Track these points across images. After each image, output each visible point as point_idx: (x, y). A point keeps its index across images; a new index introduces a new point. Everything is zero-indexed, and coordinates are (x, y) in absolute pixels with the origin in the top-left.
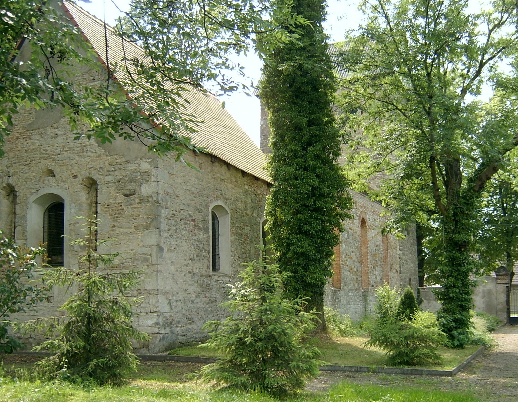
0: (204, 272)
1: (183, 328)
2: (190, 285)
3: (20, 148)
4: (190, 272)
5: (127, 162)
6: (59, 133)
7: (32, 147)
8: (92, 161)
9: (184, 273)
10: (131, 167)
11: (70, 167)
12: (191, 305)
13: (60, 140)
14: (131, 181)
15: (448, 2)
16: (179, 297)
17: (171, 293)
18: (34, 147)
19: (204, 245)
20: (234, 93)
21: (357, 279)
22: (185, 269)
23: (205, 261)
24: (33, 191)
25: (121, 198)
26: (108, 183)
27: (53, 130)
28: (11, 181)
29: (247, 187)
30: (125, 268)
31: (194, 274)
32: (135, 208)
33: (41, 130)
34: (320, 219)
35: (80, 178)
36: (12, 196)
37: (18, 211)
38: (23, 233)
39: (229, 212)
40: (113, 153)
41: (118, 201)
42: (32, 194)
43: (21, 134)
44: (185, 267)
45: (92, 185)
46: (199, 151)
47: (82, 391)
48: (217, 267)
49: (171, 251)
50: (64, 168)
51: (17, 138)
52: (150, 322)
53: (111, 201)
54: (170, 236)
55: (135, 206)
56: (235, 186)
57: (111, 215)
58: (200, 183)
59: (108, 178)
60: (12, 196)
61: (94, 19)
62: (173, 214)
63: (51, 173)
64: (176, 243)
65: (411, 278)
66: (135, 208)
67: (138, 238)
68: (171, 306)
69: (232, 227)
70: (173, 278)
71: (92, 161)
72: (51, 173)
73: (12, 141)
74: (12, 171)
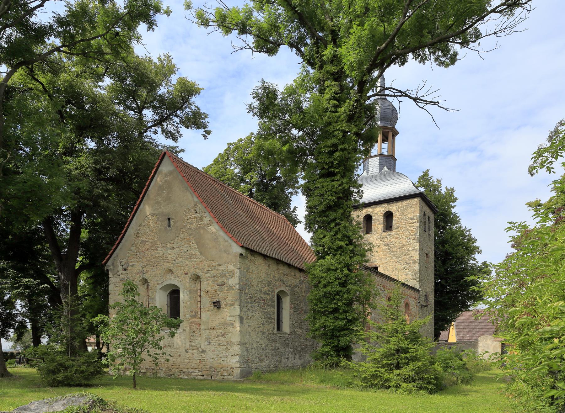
0: (271, 332)
2: (261, 339)
3: (150, 256)
4: (261, 332)
5: (220, 265)
6: (175, 246)
7: (158, 255)
8: (197, 264)
10: (222, 268)
11: (183, 268)
14: (222, 277)
15: (564, 216)
22: (257, 330)
23: (272, 324)
24: (160, 282)
25: (216, 287)
26: (207, 278)
27: (171, 245)
28: (145, 276)
29: (302, 278)
30: (219, 329)
35: (189, 275)
36: (146, 285)
37: (150, 294)
42: (158, 284)
43: (150, 247)
45: (197, 278)
48: (281, 328)
49: (248, 319)
50: (179, 268)
51: (148, 250)
52: (234, 361)
53: (210, 289)
57: (209, 297)
59: (207, 275)
60: (146, 285)
61: (427, 222)
63: (170, 271)
68: (248, 352)
70: (250, 335)
71: (197, 264)
72: (170, 271)
73: (399, 254)
74: (145, 270)
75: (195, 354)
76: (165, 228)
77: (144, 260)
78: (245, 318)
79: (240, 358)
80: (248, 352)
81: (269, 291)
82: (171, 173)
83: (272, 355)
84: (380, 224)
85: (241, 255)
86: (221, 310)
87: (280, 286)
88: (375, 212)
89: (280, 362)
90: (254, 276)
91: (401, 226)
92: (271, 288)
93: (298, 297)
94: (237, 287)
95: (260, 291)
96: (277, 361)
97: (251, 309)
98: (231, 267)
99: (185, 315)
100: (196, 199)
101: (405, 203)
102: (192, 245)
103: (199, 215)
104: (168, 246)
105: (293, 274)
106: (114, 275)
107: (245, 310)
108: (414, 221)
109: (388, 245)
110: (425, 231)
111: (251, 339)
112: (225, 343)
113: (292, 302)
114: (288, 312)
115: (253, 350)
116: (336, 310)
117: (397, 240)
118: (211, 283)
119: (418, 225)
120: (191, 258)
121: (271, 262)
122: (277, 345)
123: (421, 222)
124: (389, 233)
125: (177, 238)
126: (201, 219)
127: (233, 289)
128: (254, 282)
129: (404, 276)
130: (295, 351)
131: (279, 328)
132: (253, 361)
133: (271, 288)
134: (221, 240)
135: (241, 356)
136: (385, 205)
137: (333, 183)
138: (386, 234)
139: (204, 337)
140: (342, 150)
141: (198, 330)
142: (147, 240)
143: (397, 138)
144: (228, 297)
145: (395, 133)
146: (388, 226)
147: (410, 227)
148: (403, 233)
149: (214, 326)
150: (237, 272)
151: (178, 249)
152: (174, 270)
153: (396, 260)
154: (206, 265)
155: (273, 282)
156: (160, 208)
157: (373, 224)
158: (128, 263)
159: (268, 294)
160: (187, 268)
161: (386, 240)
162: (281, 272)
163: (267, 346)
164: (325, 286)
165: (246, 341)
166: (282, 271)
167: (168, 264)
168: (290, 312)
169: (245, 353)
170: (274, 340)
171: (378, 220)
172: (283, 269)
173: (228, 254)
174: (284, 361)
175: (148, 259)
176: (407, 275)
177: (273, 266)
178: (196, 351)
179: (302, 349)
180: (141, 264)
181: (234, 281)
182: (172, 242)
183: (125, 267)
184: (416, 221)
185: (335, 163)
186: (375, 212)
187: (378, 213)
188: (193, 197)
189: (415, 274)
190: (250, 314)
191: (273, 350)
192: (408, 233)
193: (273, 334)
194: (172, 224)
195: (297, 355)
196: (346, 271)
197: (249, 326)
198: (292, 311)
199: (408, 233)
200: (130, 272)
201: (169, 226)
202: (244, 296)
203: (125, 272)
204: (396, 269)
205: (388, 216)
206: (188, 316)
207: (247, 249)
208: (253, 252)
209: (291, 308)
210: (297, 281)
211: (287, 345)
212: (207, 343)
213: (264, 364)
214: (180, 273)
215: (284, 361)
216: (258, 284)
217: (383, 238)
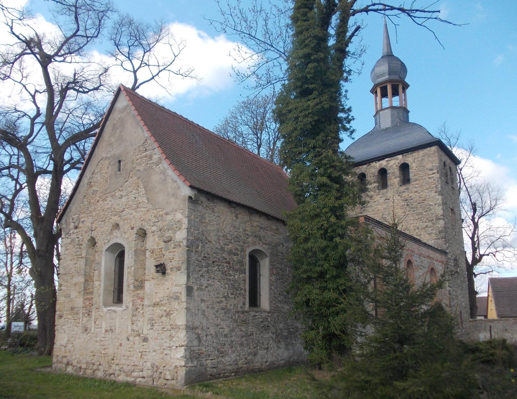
0: (239, 309)
1: (213, 361)
2: (223, 320)
5: (167, 214)
6: (123, 194)
9: (216, 309)
10: (169, 217)
12: (224, 339)
13: (124, 199)
14: (169, 229)
16: (210, 331)
17: (201, 328)
18: (108, 207)
19: (240, 284)
20: (222, 16)
21: (161, 346)
22: (217, 306)
23: (241, 298)
24: (106, 241)
25: (162, 245)
26: (153, 232)
27: (119, 193)
28: (94, 234)
30: (164, 305)
31: (228, 310)
32: (171, 252)
33: (112, 193)
34: (257, 120)
38: (99, 276)
39: (268, 255)
40: (157, 207)
41: (159, 247)
43: (100, 197)
44: (217, 304)
46: (246, 364)
47: (82, 299)
51: (98, 201)
54: (201, 276)
55: (171, 250)
56: (275, 233)
57: (155, 259)
58: (236, 230)
59: (154, 228)
61: (449, 173)
62: (205, 257)
64: (208, 282)
65: (462, 311)
66: (171, 252)
67: (172, 279)
68: (200, 341)
69: (271, 276)
73: (420, 210)
75: (137, 343)
76: (116, 173)
77: (94, 213)
78: (195, 288)
79: (186, 350)
80: (200, 341)
81: (237, 249)
82: (125, 109)
83: (242, 344)
84: (395, 178)
85: (190, 198)
86: (167, 277)
87: (254, 243)
88: (389, 165)
89: (255, 354)
90: (212, 228)
91: (419, 178)
92: (240, 246)
93: (282, 259)
94: (185, 243)
95: (222, 249)
96: (250, 354)
97: (206, 275)
98: (179, 216)
99: (128, 286)
100: (147, 134)
101: (421, 153)
102: (140, 190)
103: (148, 153)
104: (117, 195)
105: (274, 227)
106: (66, 235)
107: (195, 276)
108: (434, 172)
109: (407, 200)
110: (447, 183)
111: (205, 321)
112: (169, 327)
113: (272, 266)
114: (267, 280)
115: (209, 338)
116: (322, 275)
117: (416, 194)
118: (157, 239)
119: (438, 175)
120: (138, 208)
121: (240, 210)
122: (250, 329)
123: (442, 172)
124: (407, 186)
125: (126, 184)
126: (151, 157)
127: (180, 246)
128: (213, 237)
129: (427, 236)
130: (279, 338)
131: (254, 301)
132: (209, 355)
133: (240, 246)
134: (170, 181)
135: (188, 348)
136: (400, 157)
137: (309, 102)
138: (403, 188)
139: (147, 316)
140: (317, 61)
141: (141, 307)
142: (98, 189)
143: (408, 91)
144: (175, 257)
145: (406, 86)
146: (406, 180)
147: (429, 178)
148: (422, 186)
149: (158, 300)
150: (185, 221)
151: (126, 197)
152: (121, 224)
153: (417, 217)
154: (153, 215)
155: (243, 238)
156: (113, 149)
157: (388, 178)
158: (79, 219)
159: (235, 254)
160: (133, 221)
161: (404, 194)
162: (255, 224)
163: (233, 330)
164: (306, 240)
165: (197, 324)
166: (258, 224)
167: (115, 217)
168: (270, 280)
169: (195, 343)
170: (244, 322)
171: (393, 173)
172: (258, 221)
173: (176, 198)
174: (261, 352)
175: (97, 212)
176: (430, 234)
177: (244, 216)
178: (137, 338)
179: (290, 333)
180: (91, 220)
181: (181, 235)
182: (121, 189)
183: (76, 224)
184: (436, 171)
185: (309, 76)
186: (389, 165)
187: (392, 165)
188: (143, 132)
189: (440, 232)
190: (205, 283)
191: (243, 337)
192: (427, 186)
193: (243, 312)
194: (122, 167)
195: (283, 343)
196: (333, 219)
197: (202, 300)
198: (273, 278)
199: (427, 186)
200: (80, 230)
201: (119, 170)
202: (194, 256)
203: (76, 231)
204: (418, 228)
205: (405, 168)
206: (132, 287)
207: (200, 191)
208: (212, 197)
209: (271, 274)
210: (281, 237)
211: (266, 328)
212: (149, 327)
213: (227, 359)
214: (127, 227)
215: (261, 352)
216: (218, 239)
217: (400, 193)
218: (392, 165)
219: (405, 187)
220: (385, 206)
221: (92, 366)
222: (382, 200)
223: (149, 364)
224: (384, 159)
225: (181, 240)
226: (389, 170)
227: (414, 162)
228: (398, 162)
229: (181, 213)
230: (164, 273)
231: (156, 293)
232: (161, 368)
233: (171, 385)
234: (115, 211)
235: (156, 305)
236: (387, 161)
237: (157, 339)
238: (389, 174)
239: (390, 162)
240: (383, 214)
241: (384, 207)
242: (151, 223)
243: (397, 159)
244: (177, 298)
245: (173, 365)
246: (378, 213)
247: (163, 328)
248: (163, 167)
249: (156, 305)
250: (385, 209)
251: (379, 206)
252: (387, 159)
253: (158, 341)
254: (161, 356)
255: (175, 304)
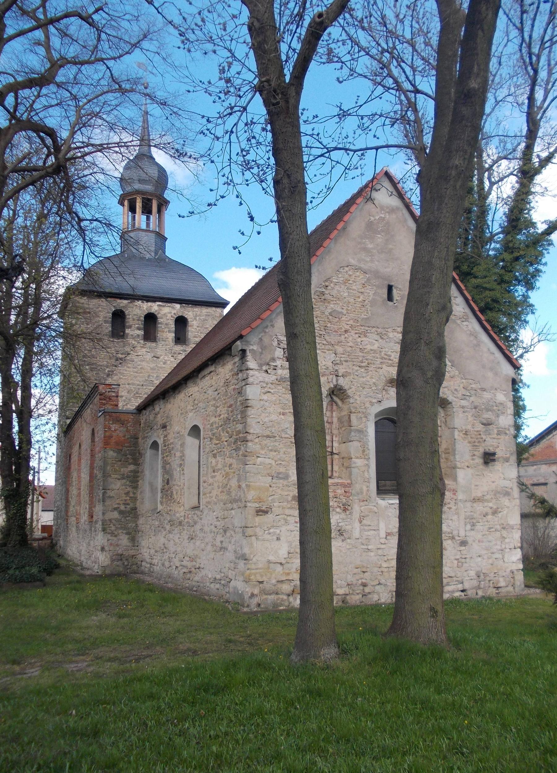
5: (483, 390)
10: (487, 395)
14: (488, 410)
25: (480, 427)
30: (487, 501)
55: (493, 436)
112: (498, 527)
136: (178, 306)
149: (479, 494)
171: (167, 324)
173: (496, 374)
212: (469, 527)
218: (167, 313)
219: (182, 348)
220: (152, 365)
221: (361, 588)
222: (149, 356)
223: (472, 573)
224: (155, 301)
225: (507, 427)
226: (162, 318)
227: (195, 319)
228: (174, 312)
229: (504, 394)
230: (486, 463)
231: (477, 486)
232: (492, 575)
233: (507, 592)
234: (390, 360)
235: (476, 500)
236: (159, 305)
237: (482, 542)
238: (161, 323)
239: (163, 308)
240: (149, 376)
241: (152, 366)
242: (460, 395)
243: (173, 308)
244: (507, 494)
245: (508, 570)
246: (141, 373)
247: (490, 528)
248: (473, 327)
249: (476, 500)
250: (152, 369)
251: (144, 364)
252: (160, 303)
253: (484, 544)
254: (490, 561)
255: (505, 501)
